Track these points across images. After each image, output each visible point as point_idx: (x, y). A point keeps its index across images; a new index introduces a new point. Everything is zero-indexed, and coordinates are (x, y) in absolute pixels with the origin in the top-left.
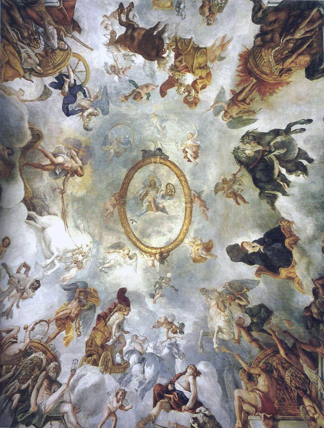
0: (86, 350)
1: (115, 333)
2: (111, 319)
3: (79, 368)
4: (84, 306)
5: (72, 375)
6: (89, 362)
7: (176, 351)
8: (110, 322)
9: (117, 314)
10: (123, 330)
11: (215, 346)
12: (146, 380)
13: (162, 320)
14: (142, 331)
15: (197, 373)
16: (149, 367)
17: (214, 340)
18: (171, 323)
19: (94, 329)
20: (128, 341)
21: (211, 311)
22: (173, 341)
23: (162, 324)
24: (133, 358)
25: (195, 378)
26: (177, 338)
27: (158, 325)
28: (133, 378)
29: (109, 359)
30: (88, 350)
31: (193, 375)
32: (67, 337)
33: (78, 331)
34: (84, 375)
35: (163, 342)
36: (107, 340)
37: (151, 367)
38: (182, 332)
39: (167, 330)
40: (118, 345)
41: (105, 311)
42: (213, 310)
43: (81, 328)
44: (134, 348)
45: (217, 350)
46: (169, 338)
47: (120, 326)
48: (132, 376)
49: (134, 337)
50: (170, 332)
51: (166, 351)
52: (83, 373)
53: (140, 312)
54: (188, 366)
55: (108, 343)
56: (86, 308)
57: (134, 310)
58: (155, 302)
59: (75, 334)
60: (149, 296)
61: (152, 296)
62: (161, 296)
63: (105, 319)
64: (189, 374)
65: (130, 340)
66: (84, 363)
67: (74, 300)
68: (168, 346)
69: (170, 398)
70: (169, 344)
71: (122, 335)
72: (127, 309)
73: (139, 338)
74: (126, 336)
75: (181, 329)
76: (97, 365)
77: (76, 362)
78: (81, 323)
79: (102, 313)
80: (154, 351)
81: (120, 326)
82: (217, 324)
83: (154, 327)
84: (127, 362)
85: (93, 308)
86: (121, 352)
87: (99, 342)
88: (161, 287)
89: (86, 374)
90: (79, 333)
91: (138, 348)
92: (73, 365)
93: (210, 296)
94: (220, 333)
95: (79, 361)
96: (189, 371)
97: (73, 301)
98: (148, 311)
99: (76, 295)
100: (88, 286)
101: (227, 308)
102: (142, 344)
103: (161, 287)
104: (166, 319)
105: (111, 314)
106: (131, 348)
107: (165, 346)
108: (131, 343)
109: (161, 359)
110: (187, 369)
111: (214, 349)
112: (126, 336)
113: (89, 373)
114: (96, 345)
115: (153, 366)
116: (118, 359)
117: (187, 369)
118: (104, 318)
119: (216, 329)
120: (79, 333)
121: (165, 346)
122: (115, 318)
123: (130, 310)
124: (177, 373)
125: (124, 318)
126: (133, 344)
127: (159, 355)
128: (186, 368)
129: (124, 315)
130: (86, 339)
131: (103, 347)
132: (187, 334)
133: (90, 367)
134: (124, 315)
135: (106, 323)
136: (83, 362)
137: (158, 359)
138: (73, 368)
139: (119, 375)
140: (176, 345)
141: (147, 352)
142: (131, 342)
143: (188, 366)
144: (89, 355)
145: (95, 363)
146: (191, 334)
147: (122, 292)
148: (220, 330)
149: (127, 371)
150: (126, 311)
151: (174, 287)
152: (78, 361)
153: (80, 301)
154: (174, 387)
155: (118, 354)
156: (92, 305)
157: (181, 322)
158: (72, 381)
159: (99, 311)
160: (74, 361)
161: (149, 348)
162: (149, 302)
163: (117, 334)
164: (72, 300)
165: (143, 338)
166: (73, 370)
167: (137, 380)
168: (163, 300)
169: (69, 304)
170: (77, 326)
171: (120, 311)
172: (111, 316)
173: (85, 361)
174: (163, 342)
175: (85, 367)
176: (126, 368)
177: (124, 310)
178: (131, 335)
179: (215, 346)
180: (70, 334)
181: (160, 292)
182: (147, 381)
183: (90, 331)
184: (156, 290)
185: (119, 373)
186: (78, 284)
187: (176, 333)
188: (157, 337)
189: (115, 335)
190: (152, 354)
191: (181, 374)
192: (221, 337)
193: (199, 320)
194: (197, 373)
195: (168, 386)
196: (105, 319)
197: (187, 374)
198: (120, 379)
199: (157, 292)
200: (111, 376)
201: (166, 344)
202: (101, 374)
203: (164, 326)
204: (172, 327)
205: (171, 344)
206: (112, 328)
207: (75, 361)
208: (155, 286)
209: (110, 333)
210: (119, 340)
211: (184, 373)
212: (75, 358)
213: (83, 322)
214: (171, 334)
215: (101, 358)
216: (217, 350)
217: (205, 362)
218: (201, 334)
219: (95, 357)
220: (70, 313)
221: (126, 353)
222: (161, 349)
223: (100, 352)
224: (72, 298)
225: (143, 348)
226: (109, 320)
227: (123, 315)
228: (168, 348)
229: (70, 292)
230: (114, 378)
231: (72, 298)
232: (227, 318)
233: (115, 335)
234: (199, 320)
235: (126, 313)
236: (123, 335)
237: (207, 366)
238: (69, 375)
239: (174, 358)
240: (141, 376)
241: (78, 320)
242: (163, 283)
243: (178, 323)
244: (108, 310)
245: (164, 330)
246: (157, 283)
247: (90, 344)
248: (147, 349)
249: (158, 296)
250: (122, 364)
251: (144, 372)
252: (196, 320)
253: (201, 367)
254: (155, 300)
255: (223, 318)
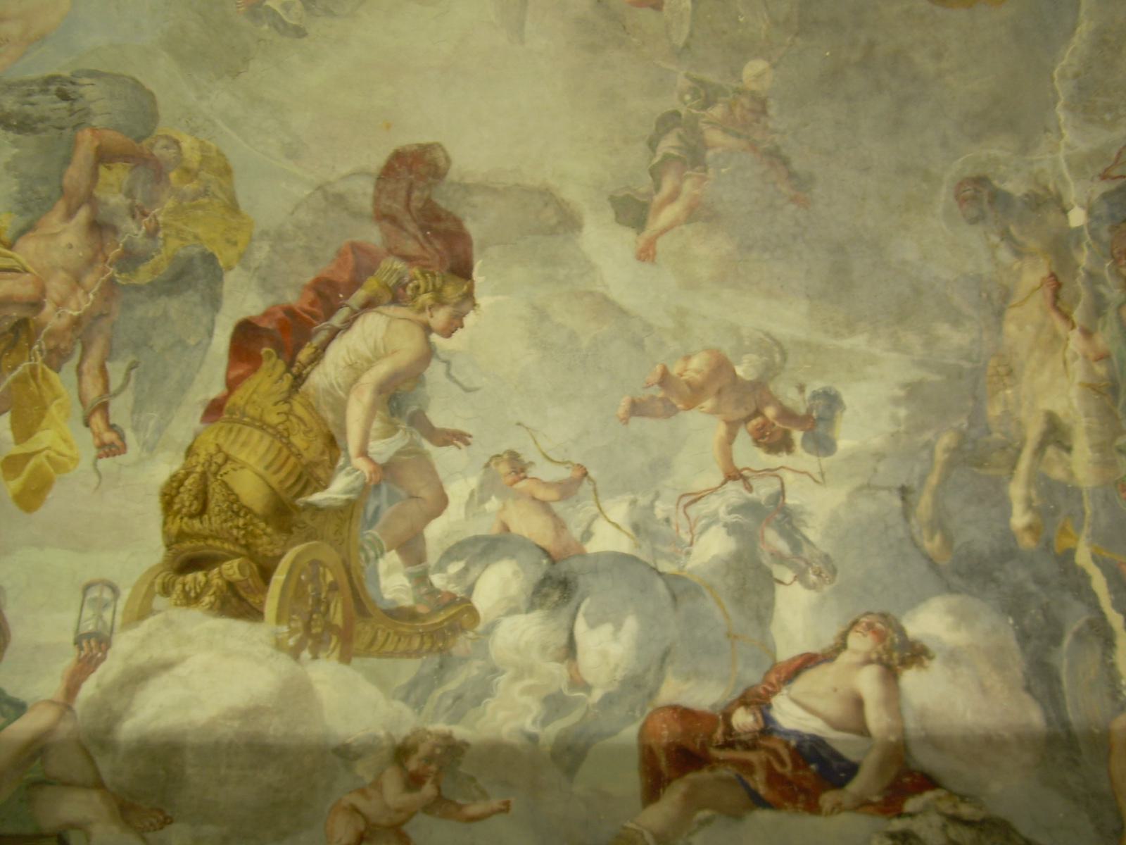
0: (166, 534)
1: (366, 437)
2: (338, 353)
3: (127, 625)
4: (130, 259)
5: (86, 666)
6: (190, 599)
7: (783, 546)
8: (327, 374)
9: (372, 326)
10: (420, 422)
11: (1020, 519)
12: (587, 688)
13: (697, 366)
14: (559, 436)
15: (900, 655)
16: (607, 629)
17: (1017, 491)
18: (757, 391)
19: (214, 410)
20: (459, 490)
21: (1010, 328)
22: (763, 490)
23: (695, 394)
24: (496, 585)
25: (890, 674)
26: (789, 477)
27: (671, 395)
28: (502, 680)
29: (334, 587)
30: (182, 536)
31: (879, 661)
32: (28, 457)
33: (97, 420)
34: (167, 666)
35: (697, 498)
36: (309, 478)
37: (618, 626)
38: (823, 445)
39: (721, 430)
40: (387, 511)
41: (291, 298)
42: (1025, 323)
43: (120, 409)
44: (506, 528)
45: (1027, 542)
46: (734, 475)
47: (398, 398)
48: (495, 671)
49: (504, 468)
50: (743, 438)
51: (713, 546)
52: (156, 652)
53: (542, 315)
54: (855, 623)
55: (317, 497)
56: (143, 275)
57: (499, 297)
58: (646, 254)
59: (84, 444)
60: (610, 214)
61: (632, 212)
62: (694, 214)
63: (289, 353)
64: (858, 658)
65: (473, 482)
66: (159, 602)
67: (61, 206)
68: (732, 518)
69: (747, 766)
70: (734, 510)
71: (413, 453)
72: (452, 291)
73: (532, 472)
74: (444, 458)
75: (816, 424)
76: (253, 613)
77: (107, 595)
78: (117, 371)
79: (267, 314)
80: (638, 546)
81: (398, 398)
82: (1045, 404)
83: (637, 408)
84: (452, 600)
85: (197, 275)
86: (411, 548)
87: (250, 486)
88: (694, 156)
89: (182, 659)
90: (109, 437)
91: (530, 525)
92: (88, 613)
93: (1014, 230)
94: (1051, 451)
95: (125, 593)
96: (860, 643)
97: (54, 220)
98: (606, 307)
99: (75, 174)
100: (154, 117)
101: (1111, 313)
102: (558, 507)
103: (694, 156)
104: (721, 366)
105: (336, 321)
106: (486, 527)
107: (713, 519)
108: (483, 501)
109: (681, 590)
110: (844, 637)
111: (1009, 535)
112: (444, 458)
113: (198, 659)
114: (236, 507)
115: (631, 624)
116: (392, 582)
117: (844, 637)
118: (279, 341)
119: (1034, 431)
120: (109, 437)
121: (713, 519)
122: (366, 345)
123: (469, 296)
124: (786, 651)
125: (429, 353)
126: (493, 504)
127: (666, 567)
128: (840, 629)
129: (427, 329)
130: (164, 468)
131: (283, 514)
132: (852, 457)
133: (201, 625)
134: (427, 329)
135: (299, 380)
136: (149, 595)
137: (660, 585)
138: (89, 627)
139: (408, 669)
140: (780, 514)
141: (592, 547)
142: (477, 499)
143: (855, 623)
144: (188, 560)
145: (238, 603)
146: (879, 456)
147: (414, 170)
148: (1056, 434)
149: (461, 644)
150: (439, 302)
151: (786, 162)
152: (115, 590)
153: (99, 228)
154: (768, 719)
155: (393, 557)
156: (190, 260)
157: (817, 385)
158: (88, 689)
159: (244, 300)
160: (94, 593)
161: (601, 528)
162: (605, 245)
163: (382, 449)
164: (45, 205)
165: (564, 473)
166: (89, 636)
167: (528, 691)
168: (707, 249)
169: (22, 233)
170: (93, 391)
171: (396, 300)
172: (334, 334)
173: (166, 590)
174: (697, 498)
175: (169, 623)
176: (455, 627)
177: (426, 298)
178: (482, 450)
179: (1020, 519)
180: (46, 438)
181: (688, 187)
182: (597, 695)
183: (186, 423)
184: (656, 174)
185: (407, 654)
186: (91, 91)
187: (782, 444)
188: (660, 467)
189: (364, 453)
190: (621, 561)
191: (808, 662)
192: (1058, 473)
193: (935, 378)
194: (900, 655)
195: (727, 716)
196: (289, 353)
197: (845, 658)
198: (413, 684)
199: (668, 185)
200: (347, 672)
201: (717, 505)
202: (284, 663)
203: (708, 404)
204: (758, 413)
205: (750, 508)
206: (340, 407)
207: (96, 590)
208: (652, 144)
209: (333, 443)
210: (405, 484)
211: (827, 657)
212: (89, 576)
213: (133, 366)
214: (747, 454)
215: (279, 577)
216: (1027, 542)
217: (954, 600)
218: (940, 456)
219: (231, 569)
220: (36, 305)
221: (450, 555)
222: (687, 538)
223: (264, 545)
224: (43, 190)
225: (560, 525)
226: (317, 357)
227: (418, 333)
228: (732, 529)
229: (29, 140)
230: (380, 682)
231: (43, 190)
232: (1100, 369)
233: (364, 453)
234: (935, 378)
235: (440, 317)
236: (423, 456)
237: (962, 618)
238: (68, 661)
239: (770, 582)
240: (558, 672)
241: (95, 353)
242: (713, 124)
243: (801, 388)
244: (311, 295)
245: (703, 428)
246: (668, 121)
247: (191, 498)
248: (588, 534)
249: (668, 215)
250: (422, 609)
251: (570, 650)
252: (916, 374)
253: (930, 622)
254: (651, 243)
255: (1078, 371)
